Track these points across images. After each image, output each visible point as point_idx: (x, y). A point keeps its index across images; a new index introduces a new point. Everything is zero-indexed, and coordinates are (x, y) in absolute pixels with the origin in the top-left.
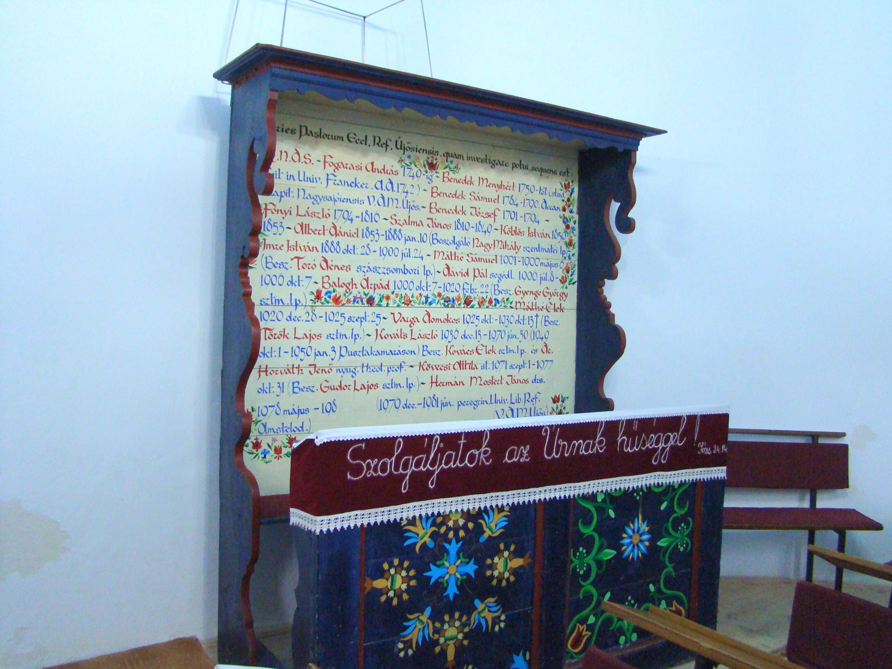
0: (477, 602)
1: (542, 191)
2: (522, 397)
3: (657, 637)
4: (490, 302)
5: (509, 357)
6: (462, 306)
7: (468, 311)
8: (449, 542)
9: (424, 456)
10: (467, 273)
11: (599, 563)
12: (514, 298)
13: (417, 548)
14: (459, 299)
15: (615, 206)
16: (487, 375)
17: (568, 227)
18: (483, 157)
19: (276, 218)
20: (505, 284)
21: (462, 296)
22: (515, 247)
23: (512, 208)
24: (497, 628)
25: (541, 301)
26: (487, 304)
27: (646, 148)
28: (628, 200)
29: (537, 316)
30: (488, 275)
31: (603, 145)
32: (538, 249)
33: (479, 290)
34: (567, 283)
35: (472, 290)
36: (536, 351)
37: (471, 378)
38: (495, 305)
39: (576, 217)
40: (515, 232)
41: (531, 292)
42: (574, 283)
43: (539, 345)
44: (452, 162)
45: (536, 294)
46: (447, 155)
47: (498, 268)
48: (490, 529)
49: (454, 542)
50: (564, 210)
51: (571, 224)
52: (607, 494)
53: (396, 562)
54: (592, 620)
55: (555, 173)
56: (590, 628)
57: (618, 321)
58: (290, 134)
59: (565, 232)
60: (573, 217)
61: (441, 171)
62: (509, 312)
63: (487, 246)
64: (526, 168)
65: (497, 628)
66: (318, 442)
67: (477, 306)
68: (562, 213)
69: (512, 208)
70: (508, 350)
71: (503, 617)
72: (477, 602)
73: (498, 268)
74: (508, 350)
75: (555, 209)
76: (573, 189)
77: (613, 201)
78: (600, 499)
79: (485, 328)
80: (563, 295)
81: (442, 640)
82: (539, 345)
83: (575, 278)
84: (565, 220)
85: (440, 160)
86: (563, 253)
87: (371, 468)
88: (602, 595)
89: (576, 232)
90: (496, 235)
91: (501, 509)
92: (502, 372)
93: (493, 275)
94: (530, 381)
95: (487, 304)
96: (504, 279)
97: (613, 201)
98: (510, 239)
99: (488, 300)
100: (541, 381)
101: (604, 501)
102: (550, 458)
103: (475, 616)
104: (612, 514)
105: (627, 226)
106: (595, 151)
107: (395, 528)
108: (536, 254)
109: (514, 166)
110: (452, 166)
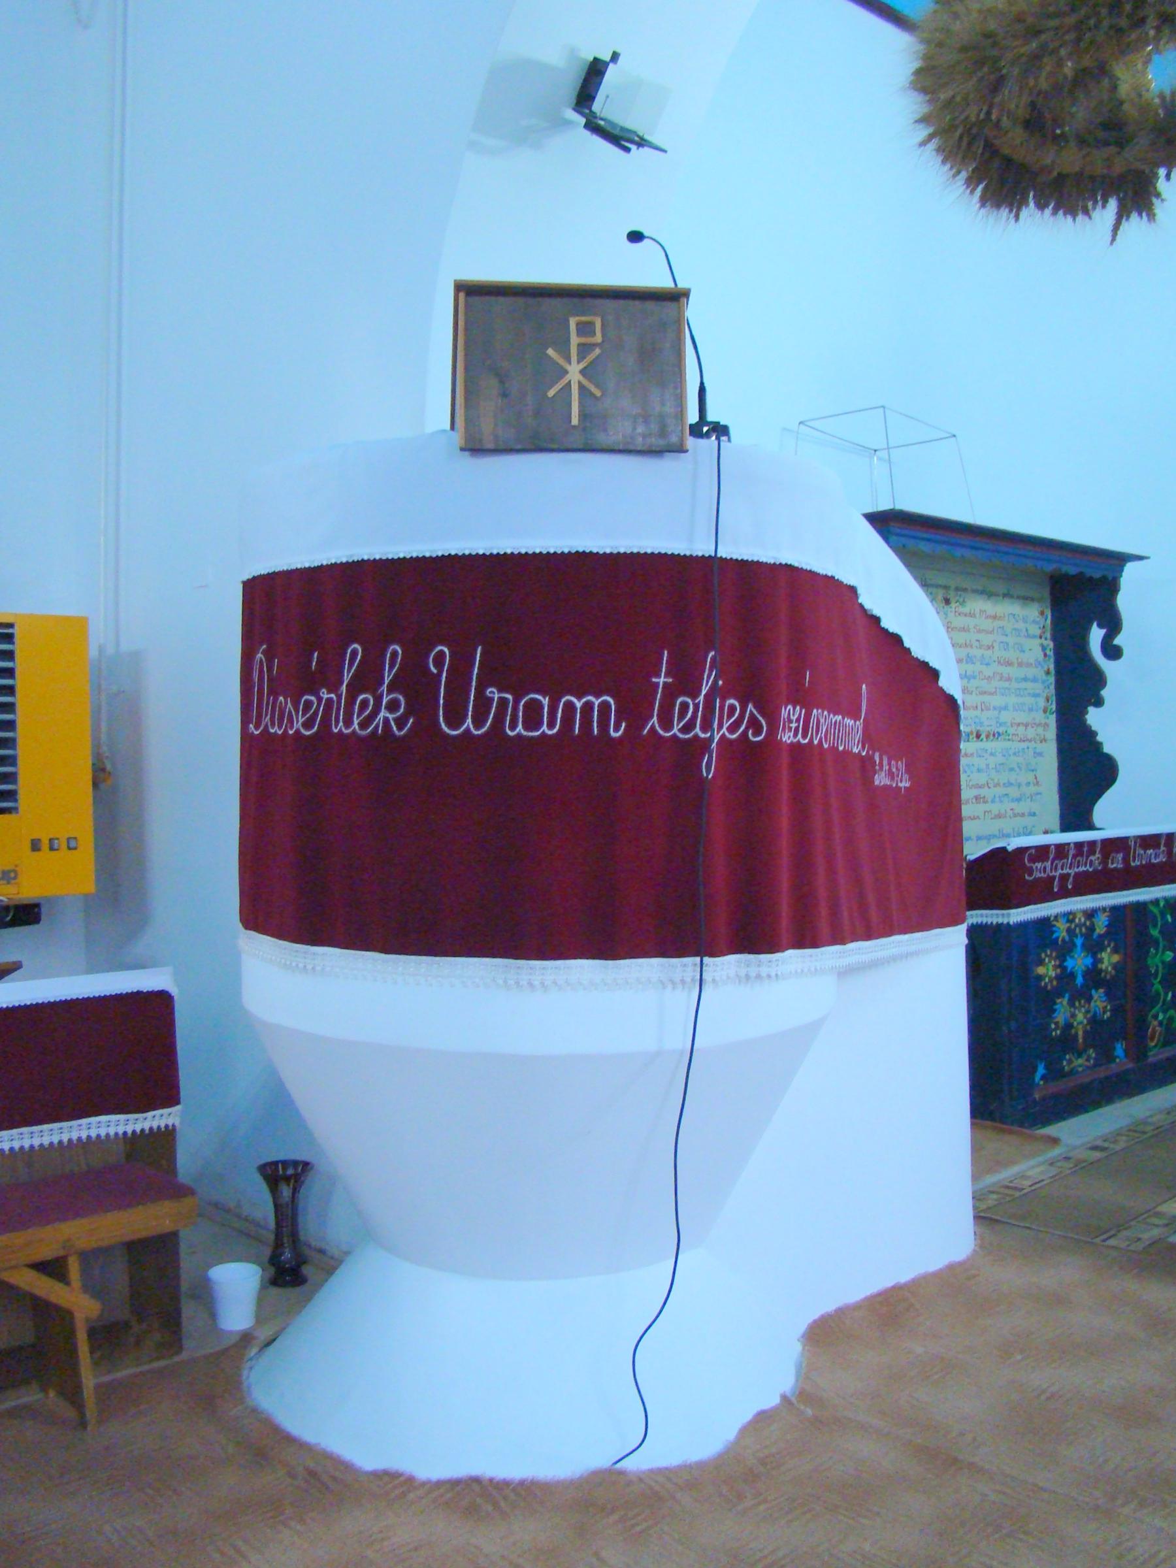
0: (1093, 992)
1: (1025, 620)
2: (1021, 830)
3: (975, 1229)
4: (994, 735)
5: (1009, 790)
6: (975, 739)
7: (980, 745)
8: (1077, 937)
9: (1066, 860)
10: (977, 707)
11: (1163, 962)
12: (1011, 731)
13: (1060, 939)
14: (972, 733)
15: (1096, 635)
16: (995, 808)
17: (1045, 655)
18: (980, 588)
19: (1031, 672)
20: (1006, 717)
21: (974, 730)
22: (1009, 679)
23: (1005, 639)
24: (1105, 1017)
25: (1031, 733)
26: (991, 737)
27: (1130, 574)
28: (1113, 624)
29: (1028, 748)
30: (992, 708)
31: (1071, 570)
32: (1025, 679)
33: (986, 723)
34: (1048, 714)
35: (981, 724)
36: (1029, 783)
37: (985, 812)
38: (998, 738)
39: (1051, 645)
40: (1009, 664)
41: (1022, 723)
42: (1053, 713)
43: (1030, 777)
44: (960, 596)
45: (1026, 725)
46: (957, 589)
47: (997, 701)
48: (1099, 928)
49: (1079, 936)
50: (1041, 637)
51: (1048, 652)
52: (1166, 899)
53: (1049, 952)
54: (1161, 1017)
55: (1032, 600)
56: (1160, 1024)
57: (1106, 749)
58: (928, 594)
59: (1044, 661)
60: (1048, 645)
61: (953, 605)
62: (1008, 744)
63: (989, 679)
64: (1011, 597)
65: (1105, 1017)
66: (1010, 848)
67: (985, 739)
68: (1038, 641)
69: (1005, 639)
70: (1010, 784)
71: (1109, 1007)
72: (1093, 992)
73: (997, 701)
74: (1010, 784)
75: (1034, 637)
76: (1047, 616)
77: (1095, 625)
78: (1162, 904)
79: (992, 761)
80: (1046, 725)
81: (1075, 1023)
82: (1030, 777)
83: (1054, 707)
84: (1044, 648)
85: (951, 595)
86: (1043, 682)
87: (1039, 870)
88: (1166, 994)
89: (1052, 660)
90: (995, 667)
91: (1104, 909)
92: (1006, 806)
93: (995, 708)
94: (1026, 814)
95: (991, 737)
96: (1003, 712)
97: (1095, 625)
98: (1005, 670)
99: (992, 733)
100: (1034, 814)
101: (1164, 906)
102: (605, 698)
103: (1092, 1004)
104: (1170, 920)
105: (1113, 652)
106: (1066, 577)
107: (1045, 924)
108: (1023, 685)
109: (1005, 596)
110: (961, 600)
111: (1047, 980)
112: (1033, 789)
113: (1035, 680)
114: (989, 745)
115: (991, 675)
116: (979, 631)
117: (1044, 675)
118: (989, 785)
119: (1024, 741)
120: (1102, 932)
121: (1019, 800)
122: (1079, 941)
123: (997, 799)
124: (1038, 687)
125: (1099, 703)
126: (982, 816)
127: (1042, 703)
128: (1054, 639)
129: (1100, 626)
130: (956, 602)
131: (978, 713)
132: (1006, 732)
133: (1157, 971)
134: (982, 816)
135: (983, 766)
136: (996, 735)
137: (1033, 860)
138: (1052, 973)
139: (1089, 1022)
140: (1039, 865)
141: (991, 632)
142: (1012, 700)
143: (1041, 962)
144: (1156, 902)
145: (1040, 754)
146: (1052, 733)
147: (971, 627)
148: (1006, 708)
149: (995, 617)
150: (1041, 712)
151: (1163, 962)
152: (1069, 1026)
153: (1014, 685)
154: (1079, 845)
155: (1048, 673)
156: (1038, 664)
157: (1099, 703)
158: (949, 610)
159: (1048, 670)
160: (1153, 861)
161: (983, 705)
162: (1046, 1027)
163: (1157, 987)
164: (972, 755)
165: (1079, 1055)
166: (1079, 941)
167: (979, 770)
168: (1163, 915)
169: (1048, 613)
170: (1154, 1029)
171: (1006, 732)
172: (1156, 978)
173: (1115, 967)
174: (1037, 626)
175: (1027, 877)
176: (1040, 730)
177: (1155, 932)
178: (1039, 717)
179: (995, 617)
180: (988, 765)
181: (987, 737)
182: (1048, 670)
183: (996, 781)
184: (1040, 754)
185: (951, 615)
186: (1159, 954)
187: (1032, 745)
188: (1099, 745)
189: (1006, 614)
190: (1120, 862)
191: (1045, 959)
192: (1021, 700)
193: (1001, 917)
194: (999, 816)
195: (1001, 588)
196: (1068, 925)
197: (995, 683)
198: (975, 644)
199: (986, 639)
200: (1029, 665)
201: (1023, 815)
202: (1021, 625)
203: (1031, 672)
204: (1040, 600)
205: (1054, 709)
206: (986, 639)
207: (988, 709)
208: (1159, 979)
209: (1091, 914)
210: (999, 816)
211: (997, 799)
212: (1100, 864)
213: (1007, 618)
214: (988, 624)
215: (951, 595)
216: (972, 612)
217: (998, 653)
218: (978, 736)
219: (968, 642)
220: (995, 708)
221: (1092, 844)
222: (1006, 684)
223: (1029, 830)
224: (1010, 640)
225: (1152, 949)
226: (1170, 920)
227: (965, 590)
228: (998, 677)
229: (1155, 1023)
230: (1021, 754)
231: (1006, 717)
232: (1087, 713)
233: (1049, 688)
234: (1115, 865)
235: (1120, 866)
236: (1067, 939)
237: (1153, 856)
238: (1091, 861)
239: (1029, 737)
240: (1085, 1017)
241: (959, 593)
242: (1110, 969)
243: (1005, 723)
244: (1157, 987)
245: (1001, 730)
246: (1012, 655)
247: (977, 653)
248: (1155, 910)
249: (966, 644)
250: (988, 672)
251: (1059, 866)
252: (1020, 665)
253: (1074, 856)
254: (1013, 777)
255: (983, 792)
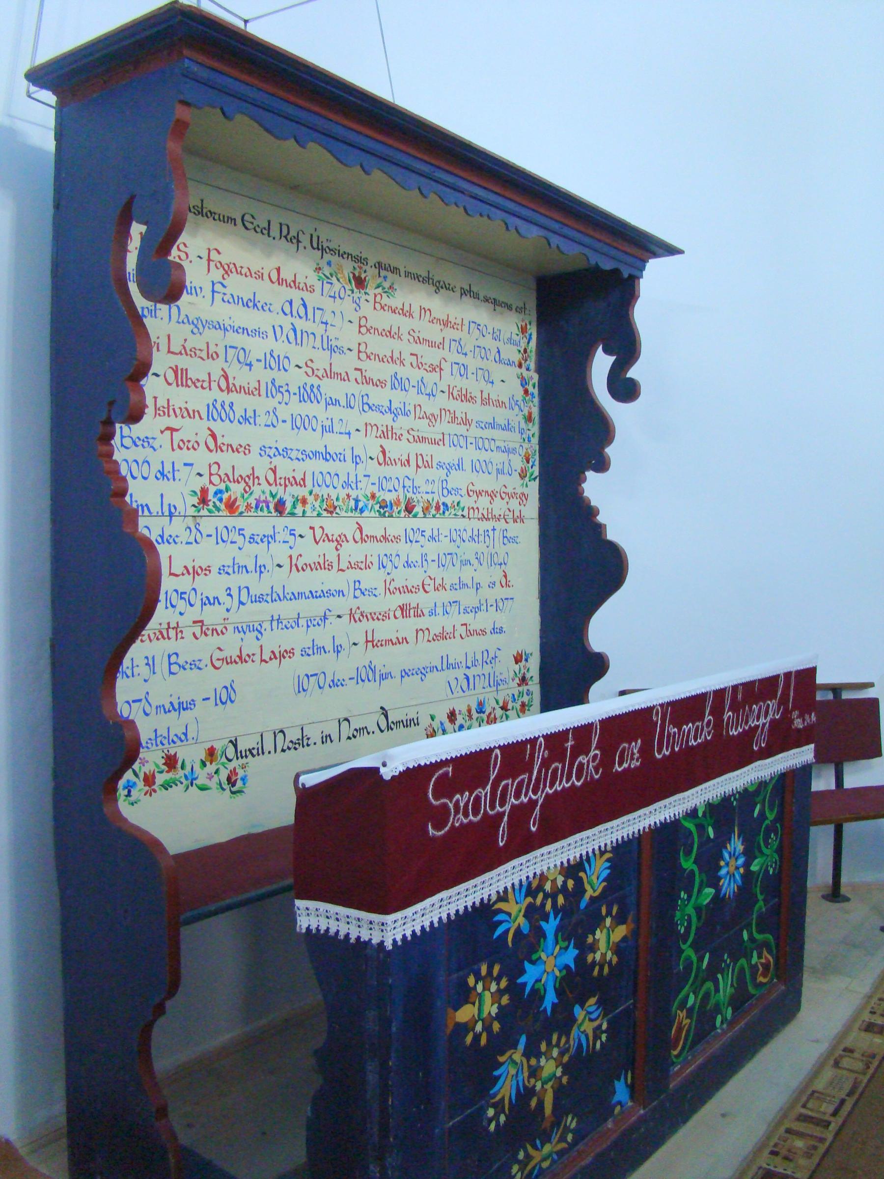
2: (479, 657)
4: (438, 508)
6: (403, 514)
7: (411, 523)
9: (525, 776)
10: (408, 461)
16: (435, 624)
17: (526, 392)
19: (502, 415)
20: (458, 480)
22: (466, 422)
23: (461, 359)
25: (499, 507)
29: (494, 530)
30: (435, 465)
32: (493, 425)
33: (423, 489)
34: (527, 479)
39: (536, 377)
40: (466, 397)
42: (535, 479)
43: (497, 574)
45: (492, 495)
50: (520, 366)
51: (530, 389)
56: (690, 1011)
57: (611, 535)
59: (524, 400)
60: (532, 378)
62: (461, 523)
63: (432, 418)
64: (476, 297)
66: (387, 773)
67: (421, 514)
69: (461, 359)
71: (605, 1026)
73: (445, 454)
74: (463, 585)
75: (510, 363)
76: (531, 335)
77: (600, 350)
79: (432, 550)
80: (524, 497)
83: (536, 471)
84: (524, 382)
85: (370, 274)
88: (701, 959)
89: (536, 400)
90: (442, 401)
92: (455, 619)
93: (440, 466)
94: (488, 631)
95: (433, 511)
98: (460, 408)
100: (501, 630)
103: (574, 1032)
104: (712, 835)
108: (488, 433)
109: (464, 293)
110: (386, 285)
111: (479, 1027)
112: (500, 592)
113: (507, 428)
114: (428, 524)
115: (437, 412)
116: (418, 341)
117: (522, 422)
118: (427, 588)
119: (488, 519)
120: (596, 894)
121: (477, 610)
122: (550, 926)
123: (439, 610)
124: (513, 439)
125: (602, 465)
126: (411, 638)
127: (518, 463)
128: (540, 369)
129: (606, 351)
130: (378, 287)
131: (410, 471)
132: (458, 503)
133: (688, 929)
134: (411, 638)
135: (415, 557)
136: (441, 508)
137: (446, 788)
138: (491, 1009)
139: (566, 1069)
140: (462, 798)
141: (440, 345)
142: (470, 454)
143: (464, 996)
144: (692, 814)
145: (513, 540)
146: (532, 509)
147: (404, 331)
148: (459, 466)
149: (446, 323)
150: (516, 475)
151: (698, 910)
152: (525, 1094)
153: (475, 432)
154: (555, 740)
155: (529, 419)
156: (513, 404)
157: (602, 465)
158: (364, 297)
159: (530, 414)
160: (692, 743)
161: (420, 458)
162: (477, 1120)
163: (689, 952)
164: (397, 538)
165: (547, 1139)
166: (550, 926)
167: (408, 564)
168: (701, 828)
169: (533, 330)
170: (680, 1023)
171: (458, 503)
172: (685, 939)
173: (618, 949)
174: (515, 348)
175: (431, 831)
176: (514, 504)
177: (688, 864)
178: (514, 483)
179: (446, 323)
180: (424, 557)
181: (426, 510)
182: (530, 414)
183: (439, 581)
184: (513, 540)
185: (367, 309)
186: (694, 898)
187: (502, 524)
188: (599, 529)
189: (466, 322)
190: (636, 756)
191: (475, 988)
192: (484, 456)
193: (366, 926)
194: (442, 636)
195: (457, 278)
196: (529, 899)
197: (444, 427)
198: (409, 359)
199: (431, 356)
200: (501, 404)
201: (483, 632)
202: (488, 342)
203: (502, 415)
204: (521, 310)
205: (536, 473)
206: (431, 356)
207: (428, 465)
208: (689, 943)
209: (573, 870)
210: (442, 636)
211: (439, 610)
212: (596, 769)
213: (466, 328)
214: (434, 333)
215: (370, 274)
216: (407, 308)
217: (449, 379)
218: (409, 509)
219: (396, 355)
220: (440, 466)
221: (583, 732)
222: (462, 429)
223: (491, 655)
224: (473, 363)
225: (682, 893)
226: (712, 835)
227: (395, 270)
228: (448, 418)
229: (682, 1014)
230: (481, 538)
231: (458, 480)
232: (585, 480)
233: (529, 441)
234: (625, 765)
235: (635, 764)
236: (526, 929)
237: (692, 733)
238: (581, 765)
239: (496, 512)
240: (559, 1063)
241: (383, 273)
242: (609, 955)
243: (457, 490)
244: (689, 952)
245: (449, 500)
246: (473, 386)
247: (415, 375)
248: (690, 825)
249: (392, 358)
250: (431, 407)
251: (512, 790)
252: (486, 401)
253: (546, 764)
254: (467, 574)
255: (412, 599)
